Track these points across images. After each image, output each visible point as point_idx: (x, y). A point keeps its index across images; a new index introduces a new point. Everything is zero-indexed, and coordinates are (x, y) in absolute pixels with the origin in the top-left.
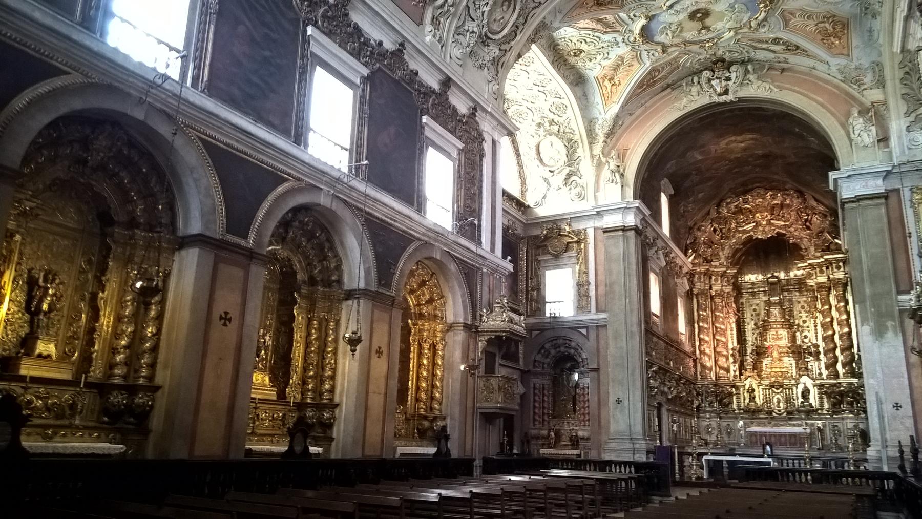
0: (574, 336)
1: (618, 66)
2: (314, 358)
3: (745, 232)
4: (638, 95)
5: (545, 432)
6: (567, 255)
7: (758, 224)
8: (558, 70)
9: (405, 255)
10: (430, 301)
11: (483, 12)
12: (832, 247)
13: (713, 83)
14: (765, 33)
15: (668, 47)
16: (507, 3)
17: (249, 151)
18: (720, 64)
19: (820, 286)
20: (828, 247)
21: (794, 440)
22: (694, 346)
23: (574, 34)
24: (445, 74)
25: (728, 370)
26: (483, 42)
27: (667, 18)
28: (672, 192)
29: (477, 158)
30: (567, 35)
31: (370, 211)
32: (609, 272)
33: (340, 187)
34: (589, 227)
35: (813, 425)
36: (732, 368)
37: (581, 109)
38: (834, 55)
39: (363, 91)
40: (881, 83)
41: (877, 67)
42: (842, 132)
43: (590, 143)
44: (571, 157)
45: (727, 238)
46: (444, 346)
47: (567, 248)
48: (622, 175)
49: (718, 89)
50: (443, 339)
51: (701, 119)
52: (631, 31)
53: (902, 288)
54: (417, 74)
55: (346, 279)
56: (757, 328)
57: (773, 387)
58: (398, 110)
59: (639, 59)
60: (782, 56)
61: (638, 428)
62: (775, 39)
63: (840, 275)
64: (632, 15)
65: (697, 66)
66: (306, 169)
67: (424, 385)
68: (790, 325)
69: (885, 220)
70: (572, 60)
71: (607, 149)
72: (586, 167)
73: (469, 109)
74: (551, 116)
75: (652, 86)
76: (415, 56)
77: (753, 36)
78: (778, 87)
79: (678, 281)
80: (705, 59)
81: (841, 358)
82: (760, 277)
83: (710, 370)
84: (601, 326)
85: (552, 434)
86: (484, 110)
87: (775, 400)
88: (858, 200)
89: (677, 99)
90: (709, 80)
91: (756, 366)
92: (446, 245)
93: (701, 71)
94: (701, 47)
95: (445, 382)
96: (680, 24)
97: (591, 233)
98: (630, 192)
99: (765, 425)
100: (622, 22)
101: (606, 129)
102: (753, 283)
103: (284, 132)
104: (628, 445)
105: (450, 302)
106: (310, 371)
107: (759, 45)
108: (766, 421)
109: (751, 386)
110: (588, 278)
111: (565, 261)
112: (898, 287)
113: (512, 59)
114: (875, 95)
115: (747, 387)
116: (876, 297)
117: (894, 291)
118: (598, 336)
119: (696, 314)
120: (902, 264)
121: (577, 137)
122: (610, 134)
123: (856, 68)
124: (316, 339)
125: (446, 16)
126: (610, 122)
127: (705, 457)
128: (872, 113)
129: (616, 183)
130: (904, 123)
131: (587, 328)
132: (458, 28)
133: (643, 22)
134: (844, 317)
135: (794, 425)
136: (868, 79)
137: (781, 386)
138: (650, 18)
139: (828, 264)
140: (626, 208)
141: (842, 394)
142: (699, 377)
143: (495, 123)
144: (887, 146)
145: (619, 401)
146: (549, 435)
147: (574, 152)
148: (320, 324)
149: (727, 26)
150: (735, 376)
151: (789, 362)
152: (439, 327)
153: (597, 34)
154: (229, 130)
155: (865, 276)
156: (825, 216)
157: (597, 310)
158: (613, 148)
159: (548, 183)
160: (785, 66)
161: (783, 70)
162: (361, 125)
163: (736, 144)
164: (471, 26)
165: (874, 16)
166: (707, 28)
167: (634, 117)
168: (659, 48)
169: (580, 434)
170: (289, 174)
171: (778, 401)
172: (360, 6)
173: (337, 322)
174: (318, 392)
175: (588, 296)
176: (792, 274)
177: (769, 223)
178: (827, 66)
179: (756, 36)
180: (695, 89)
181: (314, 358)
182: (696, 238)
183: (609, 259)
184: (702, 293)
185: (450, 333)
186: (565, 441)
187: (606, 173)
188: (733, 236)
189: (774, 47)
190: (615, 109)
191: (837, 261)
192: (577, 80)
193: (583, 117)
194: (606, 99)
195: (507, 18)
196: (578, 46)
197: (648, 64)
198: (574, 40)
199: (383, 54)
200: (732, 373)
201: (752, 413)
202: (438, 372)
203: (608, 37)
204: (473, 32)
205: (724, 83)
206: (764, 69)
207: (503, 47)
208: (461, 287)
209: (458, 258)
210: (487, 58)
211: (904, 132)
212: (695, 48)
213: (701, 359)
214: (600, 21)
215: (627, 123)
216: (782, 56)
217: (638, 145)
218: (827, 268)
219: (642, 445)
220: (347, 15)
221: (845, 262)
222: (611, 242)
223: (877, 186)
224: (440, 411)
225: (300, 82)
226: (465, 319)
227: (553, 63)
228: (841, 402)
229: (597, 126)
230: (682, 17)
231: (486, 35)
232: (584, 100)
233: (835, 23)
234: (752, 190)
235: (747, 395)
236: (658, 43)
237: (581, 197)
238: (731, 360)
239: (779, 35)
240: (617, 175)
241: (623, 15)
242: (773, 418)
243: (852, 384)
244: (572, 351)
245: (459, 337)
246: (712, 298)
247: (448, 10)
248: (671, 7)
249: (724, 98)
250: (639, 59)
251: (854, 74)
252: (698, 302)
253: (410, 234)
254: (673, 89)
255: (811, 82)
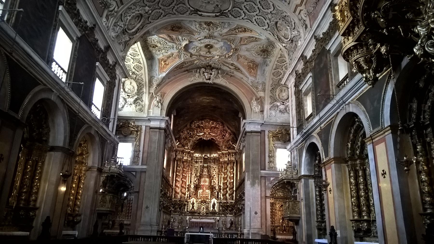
0: (129, 175)
1: (170, 57)
2: (27, 181)
3: (199, 136)
4: (174, 71)
5: (107, 221)
6: (131, 136)
7: (205, 133)
8: (144, 51)
9: (81, 131)
10: (82, 154)
11: (127, 19)
12: (232, 147)
13: (205, 74)
14: (230, 61)
15: (193, 55)
16: (137, 18)
17: (26, 66)
18: (209, 67)
19: (225, 162)
20: (230, 147)
21: (208, 225)
22: (173, 183)
23: (157, 38)
24: (108, 43)
25: (185, 194)
26: (124, 32)
27: (196, 44)
28: (175, 115)
29: (113, 87)
30: (154, 39)
31: (71, 107)
32: (150, 147)
33: (63, 92)
34: (143, 125)
35: (216, 219)
36: (187, 193)
37: (148, 71)
38: (251, 76)
39: (77, 44)
40: (264, 90)
41: (264, 84)
42: (249, 105)
43: (149, 87)
44: (139, 92)
45: (192, 137)
46: (85, 178)
47: (131, 133)
48: (162, 104)
49: (207, 77)
50: (84, 174)
51: (197, 87)
52: (181, 45)
53: (262, 168)
54: (98, 41)
55: (51, 140)
56: (197, 177)
57: (202, 202)
58: (90, 58)
59: (180, 57)
60: (232, 71)
61: (154, 221)
62: (232, 64)
63: (233, 159)
64: (183, 38)
65: (200, 66)
66: (50, 80)
67: (72, 198)
68: (210, 177)
69: (260, 141)
70: (151, 49)
71: (156, 91)
72: (146, 98)
73: (113, 62)
74: (134, 70)
75: (182, 69)
76: (98, 32)
77: (225, 60)
78: (229, 82)
79: (172, 153)
80: (204, 64)
81: (229, 192)
82: (200, 155)
83: (178, 194)
84: (143, 172)
85: (111, 223)
86: (120, 65)
87: (202, 208)
88: (252, 133)
89: (189, 77)
90: (204, 73)
91: (196, 194)
92: (98, 128)
93: (201, 68)
94: (205, 59)
95: (83, 197)
96: (200, 48)
97: (144, 128)
98: (164, 113)
99: (197, 219)
100: (178, 40)
101: (158, 82)
102: (197, 158)
103: (43, 58)
104: (149, 228)
105: (91, 156)
106: (24, 189)
107: (226, 64)
108: (198, 217)
109: (193, 202)
110: (139, 148)
111: (129, 139)
112: (261, 167)
113: (132, 43)
114: (261, 94)
115: (191, 202)
116: (253, 170)
117: (260, 168)
118: (140, 177)
119: (175, 168)
120: (263, 159)
121: (144, 83)
122: (158, 85)
123: (257, 83)
124: (30, 171)
125: (112, 16)
126: (160, 80)
127: (186, 233)
128: (259, 100)
129: (159, 107)
130: (269, 106)
131: (136, 172)
132: (115, 23)
133: (187, 42)
134: (232, 175)
135: (209, 219)
136: (260, 88)
137: (205, 202)
138: (190, 42)
139: (229, 154)
140: (162, 119)
141: (228, 206)
142: (173, 196)
143: (122, 71)
144: (263, 114)
145: (147, 207)
146: (109, 223)
147: (141, 89)
148: (33, 163)
149: (217, 54)
150: (187, 197)
151: (208, 191)
152: (84, 168)
153: (166, 41)
154: (21, 53)
155: (251, 162)
156: (231, 135)
157: (142, 164)
158: (159, 91)
159: (126, 101)
160: (232, 74)
161: (231, 76)
162: (73, 61)
163: (205, 100)
164: (121, 24)
165: (266, 66)
166: (209, 52)
167: (170, 80)
168: (189, 55)
169: (125, 222)
170: (42, 82)
171: (203, 210)
172: (82, 2)
173: (43, 163)
174: (28, 201)
175: (138, 157)
176: (212, 156)
177: (209, 134)
178: (247, 79)
179: (226, 61)
180: (197, 75)
181: (27, 181)
182: (180, 135)
183: (150, 140)
184: (180, 160)
185: (89, 172)
186: (117, 226)
187: (155, 102)
188: (195, 137)
189: (230, 67)
190: (164, 74)
191: (233, 153)
192: (150, 58)
193: (148, 74)
194: (161, 69)
195: (135, 25)
196: (156, 43)
197: (183, 59)
198: (156, 41)
199: (86, 28)
200: (186, 195)
201: (193, 213)
202: (80, 191)
203: (171, 44)
204: (121, 27)
205: (209, 75)
206: (225, 74)
207: (131, 37)
208: (99, 149)
209: (100, 135)
210: (123, 40)
211: (269, 110)
212: (203, 58)
213: (175, 188)
214: (169, 36)
215: (167, 82)
216: (232, 71)
217: (171, 92)
218: (228, 155)
219: (155, 228)
220: (75, 4)
221: (235, 153)
222: (153, 133)
223: (258, 128)
224: (78, 211)
225: (52, 34)
226: (98, 165)
227: (142, 48)
228: (227, 210)
229: (154, 80)
230: (202, 45)
231: (125, 30)
232: (151, 67)
233: (254, 64)
234: (205, 119)
235: (191, 206)
236: (190, 53)
237: (141, 110)
238: (187, 190)
239: (234, 63)
240: (160, 104)
241: (180, 37)
242: (201, 216)
243: (232, 202)
244: (126, 182)
245: (95, 174)
246: (183, 162)
247: (114, 14)
248: (200, 40)
249: (208, 81)
250: (180, 57)
251: (256, 84)
252: (177, 163)
253: (85, 121)
254: (188, 72)
255: (240, 83)
